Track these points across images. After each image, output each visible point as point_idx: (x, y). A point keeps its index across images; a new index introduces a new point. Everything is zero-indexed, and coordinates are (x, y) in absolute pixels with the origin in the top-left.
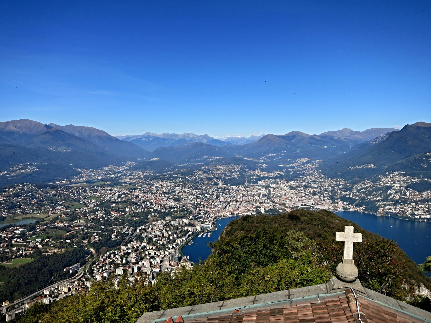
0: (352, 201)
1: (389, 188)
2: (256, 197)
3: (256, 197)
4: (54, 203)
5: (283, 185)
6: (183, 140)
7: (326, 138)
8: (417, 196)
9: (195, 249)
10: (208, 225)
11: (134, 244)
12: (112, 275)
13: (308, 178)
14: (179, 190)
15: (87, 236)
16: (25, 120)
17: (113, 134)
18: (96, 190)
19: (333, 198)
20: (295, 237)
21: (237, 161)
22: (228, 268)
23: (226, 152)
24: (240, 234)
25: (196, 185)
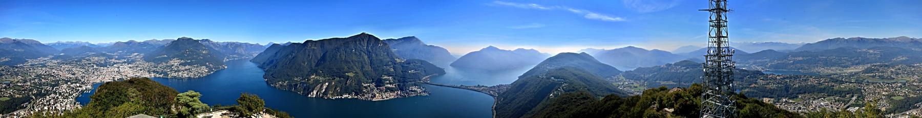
0: (157, 72)
4: (17, 75)
5: (126, 66)
6: (76, 45)
7: (145, 44)
8: (183, 68)
9: (82, 99)
10: (89, 87)
11: (53, 95)
12: (42, 110)
14: (74, 69)
15: (31, 90)
16: (829, 40)
17: (42, 43)
18: (35, 69)
19: (149, 72)
20: (132, 91)
21: (104, 55)
22: (99, 108)
23: (98, 50)
24: (105, 91)
25: (83, 67)
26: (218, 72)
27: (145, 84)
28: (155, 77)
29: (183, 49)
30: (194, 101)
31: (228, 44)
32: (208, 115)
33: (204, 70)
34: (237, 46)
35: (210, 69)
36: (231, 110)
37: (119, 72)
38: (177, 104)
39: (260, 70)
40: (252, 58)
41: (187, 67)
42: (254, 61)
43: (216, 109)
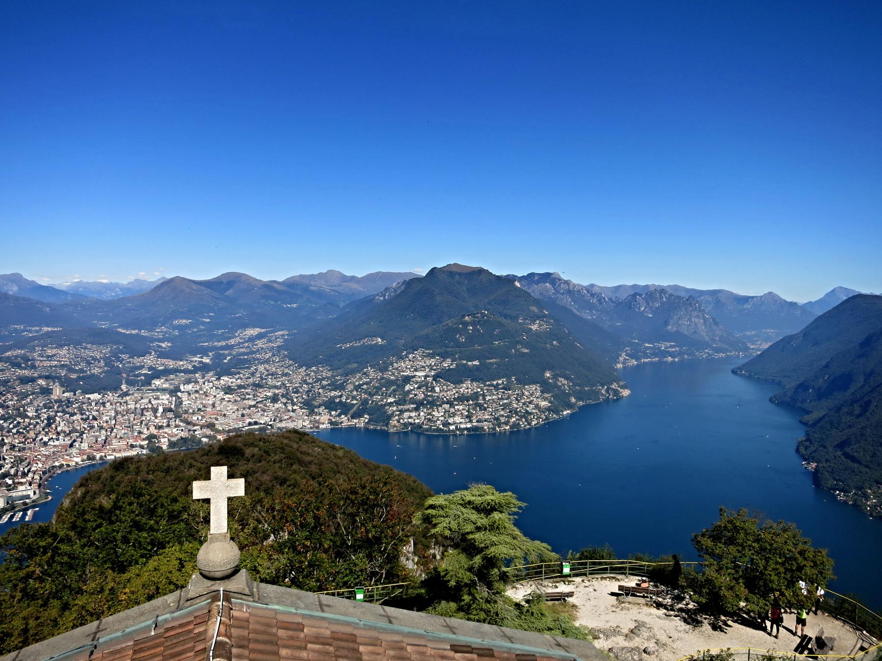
0: (345, 408)
1: (407, 380)
2: (149, 415)
3: (149, 415)
5: (210, 385)
7: (296, 288)
8: (452, 392)
10: (26, 491)
13: (261, 368)
19: (310, 406)
21: (100, 337)
26: (589, 413)
27: (292, 459)
28: (335, 429)
29: (450, 310)
30: (493, 528)
31: (637, 294)
32: (550, 588)
33: (534, 402)
34: (671, 302)
35: (560, 400)
36: (656, 576)
37: (176, 412)
38: (423, 541)
39: (783, 418)
40: (741, 358)
41: (467, 387)
42: (751, 371)
43: (590, 564)
